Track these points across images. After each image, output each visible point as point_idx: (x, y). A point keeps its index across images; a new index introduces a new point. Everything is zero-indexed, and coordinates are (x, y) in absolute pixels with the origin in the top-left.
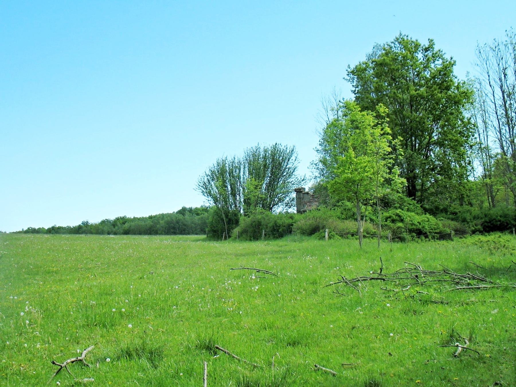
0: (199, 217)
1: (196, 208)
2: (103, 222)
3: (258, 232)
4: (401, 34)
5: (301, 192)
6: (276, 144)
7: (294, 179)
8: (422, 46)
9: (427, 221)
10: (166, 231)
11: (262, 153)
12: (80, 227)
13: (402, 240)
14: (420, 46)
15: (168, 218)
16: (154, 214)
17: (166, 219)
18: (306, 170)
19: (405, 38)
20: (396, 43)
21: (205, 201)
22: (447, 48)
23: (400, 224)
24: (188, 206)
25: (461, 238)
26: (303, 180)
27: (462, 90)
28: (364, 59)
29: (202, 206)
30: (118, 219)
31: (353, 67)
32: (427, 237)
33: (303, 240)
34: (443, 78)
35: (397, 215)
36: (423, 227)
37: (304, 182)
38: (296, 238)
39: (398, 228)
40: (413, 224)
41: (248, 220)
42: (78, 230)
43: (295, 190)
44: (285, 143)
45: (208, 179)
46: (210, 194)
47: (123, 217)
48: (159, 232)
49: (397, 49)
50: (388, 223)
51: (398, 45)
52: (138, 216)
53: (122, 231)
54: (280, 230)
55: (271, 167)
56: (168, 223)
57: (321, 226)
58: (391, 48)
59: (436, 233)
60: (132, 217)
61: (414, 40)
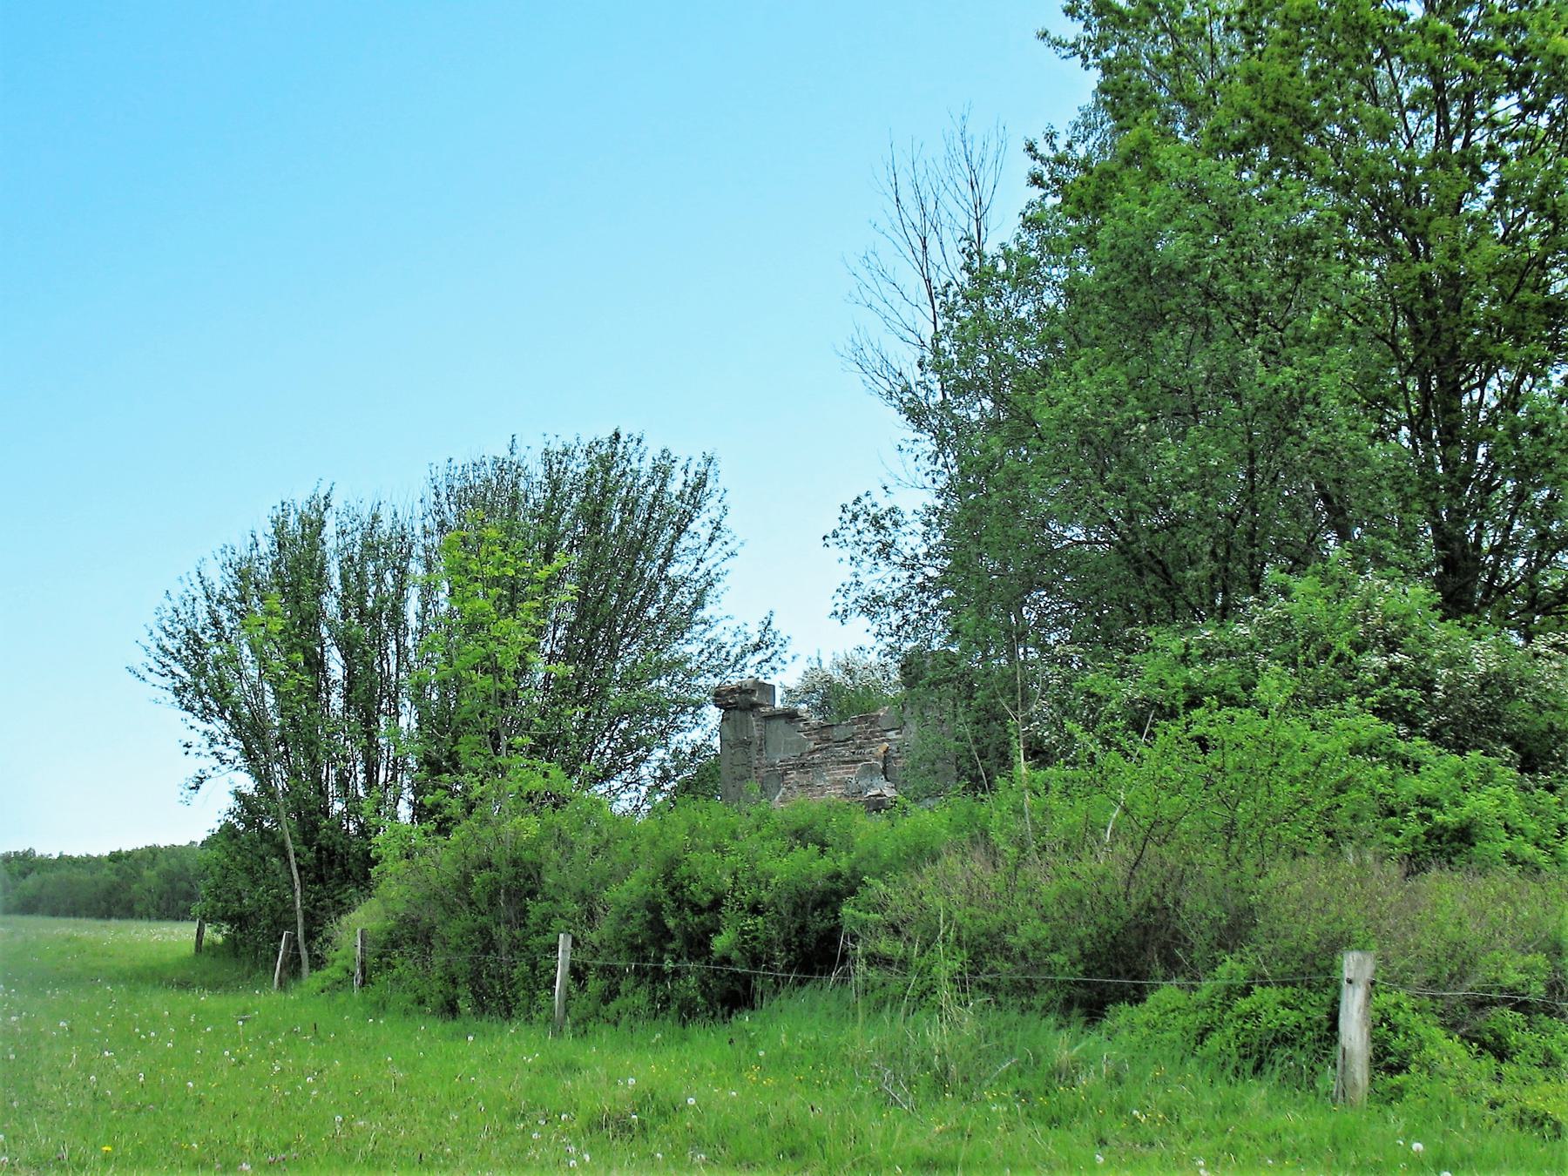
3: (517, 946)
5: (754, 706)
6: (617, 436)
10: (163, 905)
11: (538, 472)
15: (173, 861)
16: (127, 847)
17: (164, 865)
18: (802, 574)
26: (757, 648)
37: (760, 656)
41: (442, 859)
43: (722, 698)
44: (665, 430)
47: (25, 854)
48: (138, 908)
54: (720, 943)
55: (595, 553)
56: (170, 878)
57: (1199, 907)
60: (55, 856)
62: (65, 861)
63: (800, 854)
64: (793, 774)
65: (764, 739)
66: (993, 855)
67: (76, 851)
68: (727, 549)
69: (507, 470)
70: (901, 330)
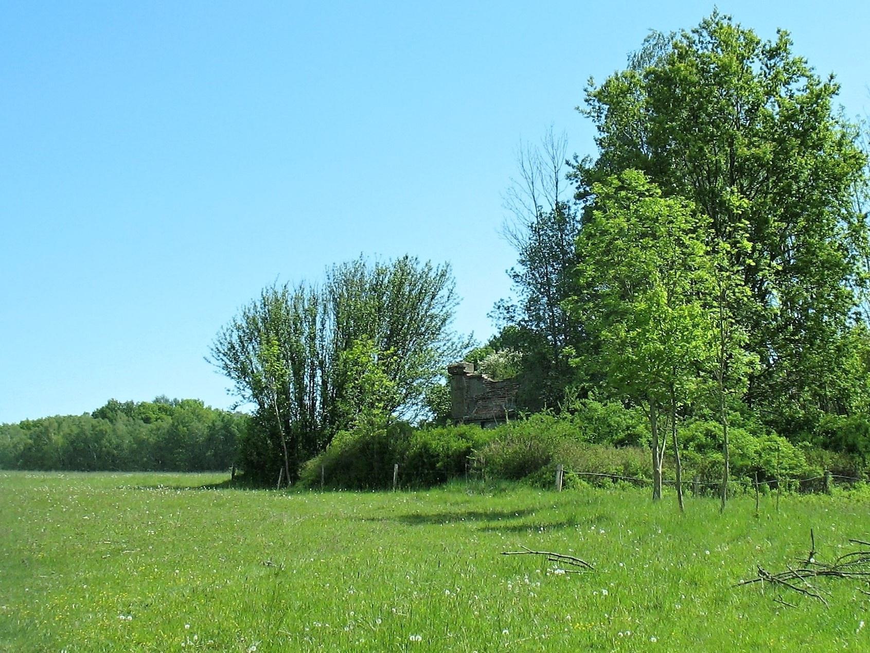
0: (149, 426)
1: (143, 405)
4: (715, 14)
7: (442, 344)
8: (762, 43)
9: (786, 452)
13: (719, 492)
14: (758, 43)
16: (33, 417)
17: (67, 430)
19: (725, 23)
20: (705, 33)
23: (718, 456)
24: (122, 400)
25: (845, 488)
27: (847, 150)
28: (623, 67)
31: (599, 84)
32: (773, 486)
33: (504, 490)
34: (805, 122)
35: (708, 433)
36: (768, 462)
38: (482, 484)
39: (714, 464)
40: (743, 456)
44: (426, 255)
45: (240, 337)
46: (243, 372)
49: (705, 48)
50: (691, 452)
51: (709, 39)
55: (393, 309)
59: (793, 476)
60: (18, 423)
61: (745, 27)
64: (480, 402)
68: (456, 301)
69: (359, 267)
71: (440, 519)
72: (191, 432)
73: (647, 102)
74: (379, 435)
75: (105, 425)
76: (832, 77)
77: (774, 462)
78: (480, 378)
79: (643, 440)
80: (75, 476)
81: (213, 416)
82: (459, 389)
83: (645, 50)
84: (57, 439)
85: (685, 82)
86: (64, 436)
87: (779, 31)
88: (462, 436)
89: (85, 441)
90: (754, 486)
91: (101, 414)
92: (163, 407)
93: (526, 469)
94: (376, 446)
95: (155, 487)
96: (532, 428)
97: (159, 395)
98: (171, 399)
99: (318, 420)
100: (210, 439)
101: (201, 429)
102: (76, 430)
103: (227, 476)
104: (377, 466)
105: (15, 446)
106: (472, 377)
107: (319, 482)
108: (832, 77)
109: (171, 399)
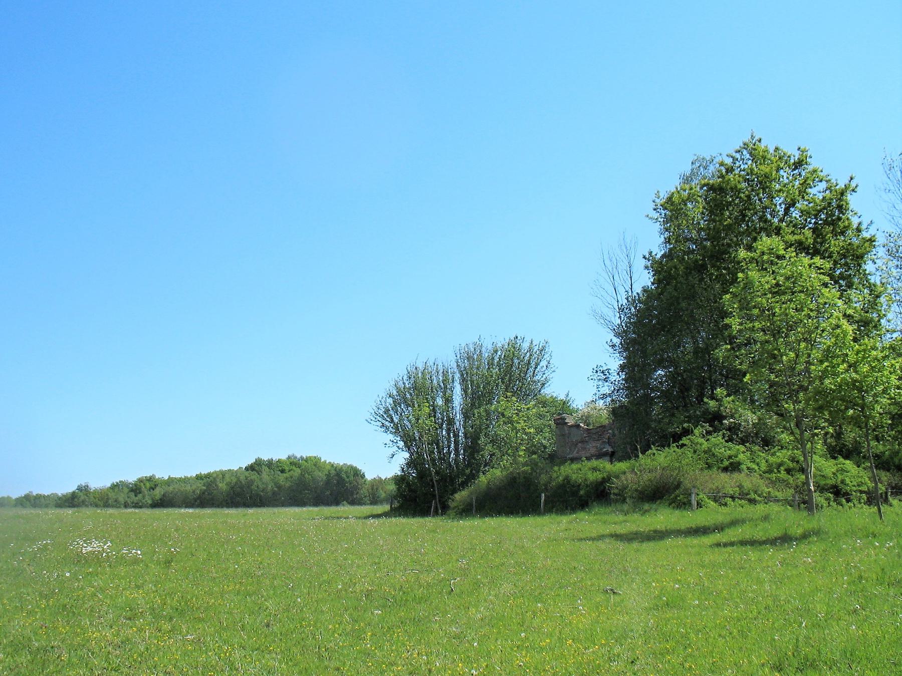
1: (279, 461)
2: (114, 487)
9: (854, 474)
12: (73, 496)
16: (205, 471)
17: (227, 479)
20: (745, 152)
21: (388, 442)
22: (832, 165)
24: (265, 458)
29: (289, 457)
30: (141, 480)
31: (664, 195)
36: (843, 482)
38: (626, 507)
42: (72, 501)
44: (531, 333)
47: (151, 477)
52: (178, 476)
53: (150, 502)
55: (507, 375)
58: (735, 160)
59: (861, 492)
62: (171, 481)
63: (595, 474)
65: (570, 434)
66: (636, 474)
67: (178, 474)
69: (479, 347)
70: (606, 257)
71: (658, 535)
72: (314, 479)
73: (704, 208)
74: (523, 472)
75: (254, 476)
76: (852, 179)
77: (848, 481)
78: (578, 426)
79: (744, 467)
80: (232, 511)
81: (328, 467)
82: (563, 435)
83: (692, 170)
84: (222, 486)
85: (736, 190)
86: (227, 484)
87: (799, 149)
88: (595, 469)
89: (242, 487)
90: (835, 501)
91: (251, 468)
92: (294, 462)
93: (660, 493)
94: (522, 480)
95: (347, 518)
96: (658, 461)
97: (291, 454)
98: (299, 456)
99: (471, 460)
100: (328, 482)
101: (321, 476)
102: (234, 480)
103: (387, 508)
104: (518, 497)
105: (194, 492)
106: (572, 426)
107: (471, 510)
108: (852, 179)
109: (299, 456)
